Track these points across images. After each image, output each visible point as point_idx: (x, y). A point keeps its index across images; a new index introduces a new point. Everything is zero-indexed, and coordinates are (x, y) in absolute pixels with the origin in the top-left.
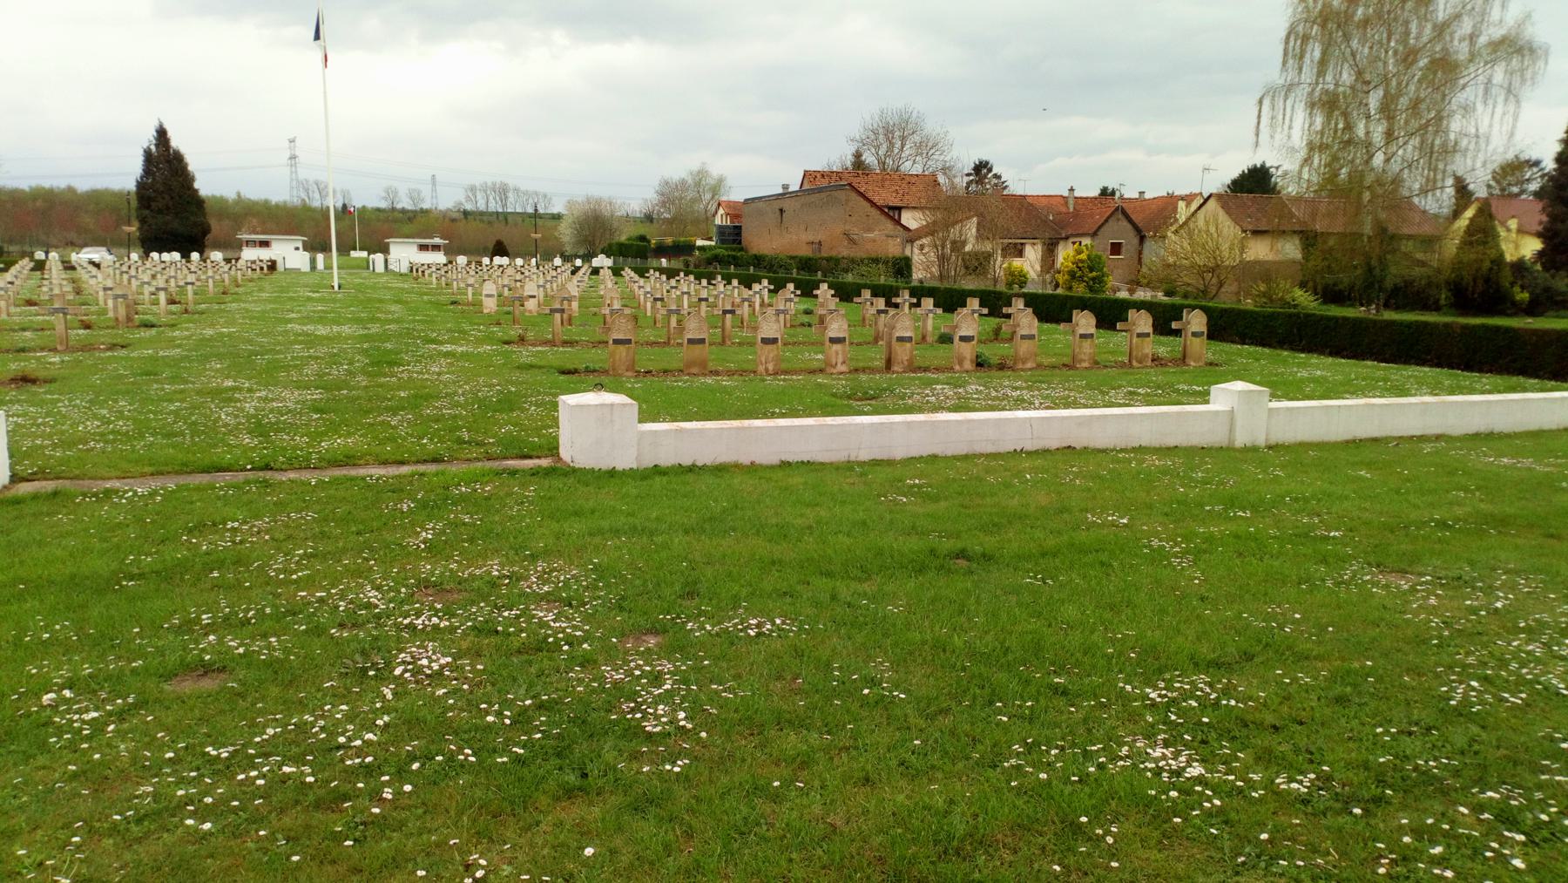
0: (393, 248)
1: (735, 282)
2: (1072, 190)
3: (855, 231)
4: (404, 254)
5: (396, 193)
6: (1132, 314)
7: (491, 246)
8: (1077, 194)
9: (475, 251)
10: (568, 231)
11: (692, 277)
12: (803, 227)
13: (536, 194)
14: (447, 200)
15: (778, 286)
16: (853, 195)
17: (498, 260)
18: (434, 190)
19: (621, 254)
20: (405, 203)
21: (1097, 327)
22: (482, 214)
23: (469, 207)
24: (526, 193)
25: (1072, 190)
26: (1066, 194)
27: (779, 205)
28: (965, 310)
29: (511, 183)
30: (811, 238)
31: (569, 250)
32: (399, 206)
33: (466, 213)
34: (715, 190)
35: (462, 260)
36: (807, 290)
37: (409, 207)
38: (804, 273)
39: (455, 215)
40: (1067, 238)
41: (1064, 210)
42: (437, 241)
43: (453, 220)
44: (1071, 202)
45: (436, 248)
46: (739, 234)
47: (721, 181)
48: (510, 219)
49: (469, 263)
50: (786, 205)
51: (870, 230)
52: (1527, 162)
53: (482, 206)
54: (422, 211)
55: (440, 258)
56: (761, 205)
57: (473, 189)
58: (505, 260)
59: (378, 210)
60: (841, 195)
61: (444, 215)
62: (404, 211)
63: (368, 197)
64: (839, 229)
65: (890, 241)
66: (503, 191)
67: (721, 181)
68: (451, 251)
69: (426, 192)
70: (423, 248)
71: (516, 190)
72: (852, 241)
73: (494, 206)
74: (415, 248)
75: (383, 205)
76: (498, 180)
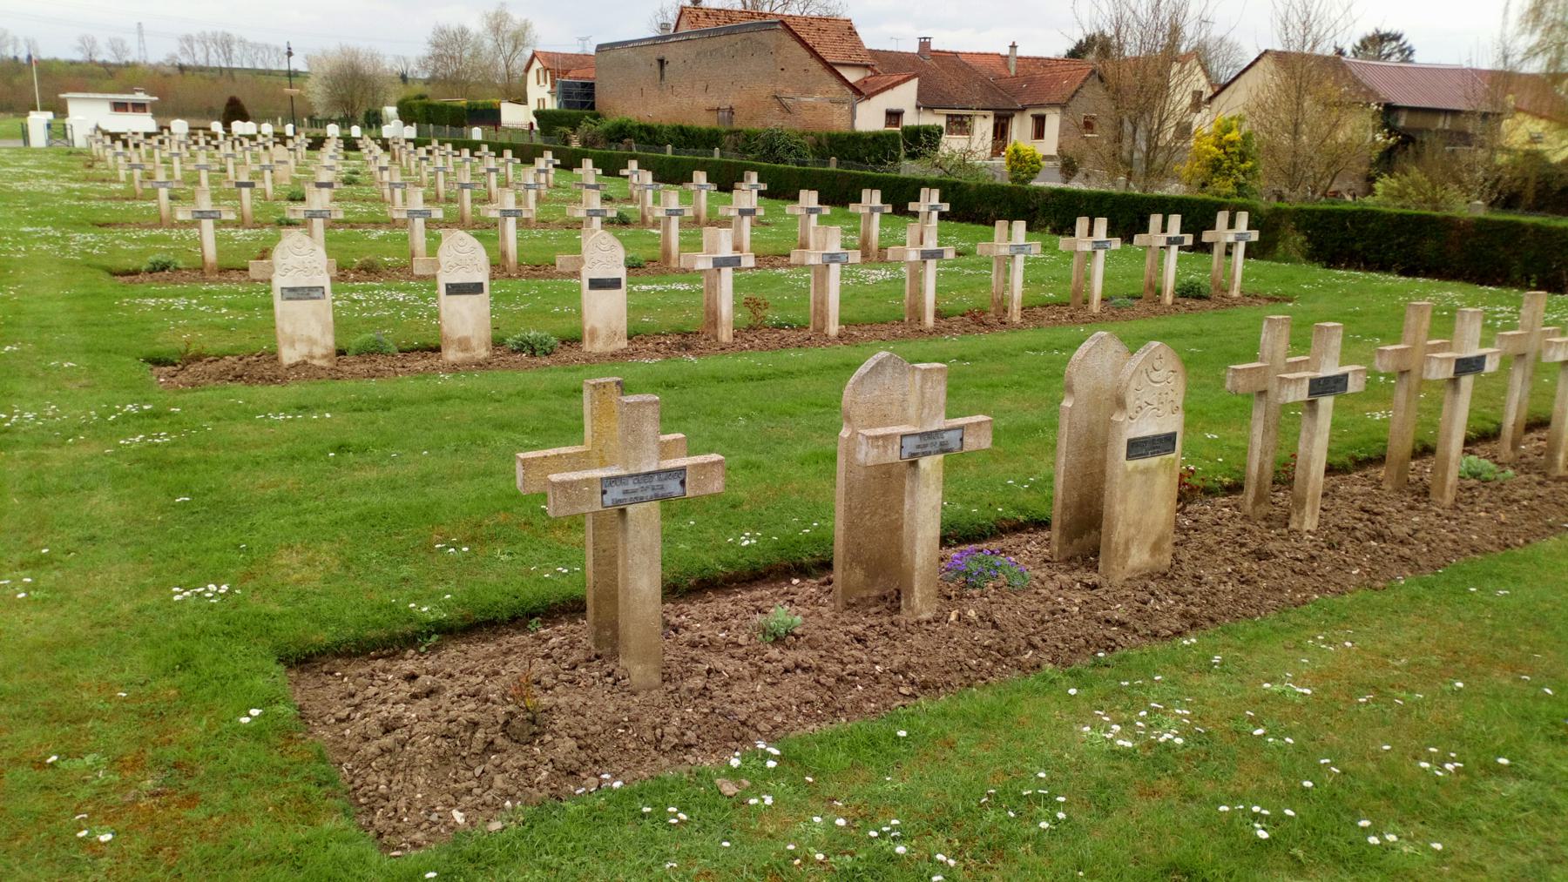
0: (72, 108)
1: (508, 154)
2: (1013, 47)
3: (788, 93)
4: (88, 115)
5: (94, 42)
6: (924, 191)
7: (221, 105)
8: (1020, 52)
9: (195, 111)
10: (319, 89)
11: (588, 171)
12: (700, 85)
13: (267, 47)
14: (158, 52)
15: (726, 181)
16: (787, 39)
17: (238, 127)
18: (141, 40)
19: (429, 121)
20: (105, 55)
21: (820, 202)
22: (201, 69)
23: (185, 61)
24: (254, 46)
25: (1013, 47)
26: (1005, 51)
27: (656, 56)
28: (744, 186)
29: (236, 33)
30: (715, 103)
31: (320, 113)
32: (99, 59)
33: (182, 68)
34: (518, 40)
35: (180, 126)
36: (611, 167)
37: (111, 60)
38: (678, 153)
39: (168, 70)
40: (1023, 109)
41: (1004, 73)
42: (140, 97)
43: (167, 76)
44: (1013, 62)
45: (139, 107)
46: (591, 95)
47: (526, 26)
48: (237, 75)
49: (192, 132)
50: (670, 53)
51: (808, 92)
52: (1387, 35)
53: (200, 60)
54: (128, 65)
55: (144, 123)
56: (625, 53)
57: (188, 39)
58: (249, 128)
59: (73, 63)
60: (766, 37)
61: (156, 69)
62: (105, 65)
63: (60, 47)
64: (764, 90)
65: (836, 109)
66: (226, 43)
67: (526, 26)
68: (161, 111)
69: (132, 42)
70: (119, 107)
71: (242, 42)
72: (786, 109)
73: (217, 61)
74: (107, 108)
75: (79, 56)
76: (220, 30)
